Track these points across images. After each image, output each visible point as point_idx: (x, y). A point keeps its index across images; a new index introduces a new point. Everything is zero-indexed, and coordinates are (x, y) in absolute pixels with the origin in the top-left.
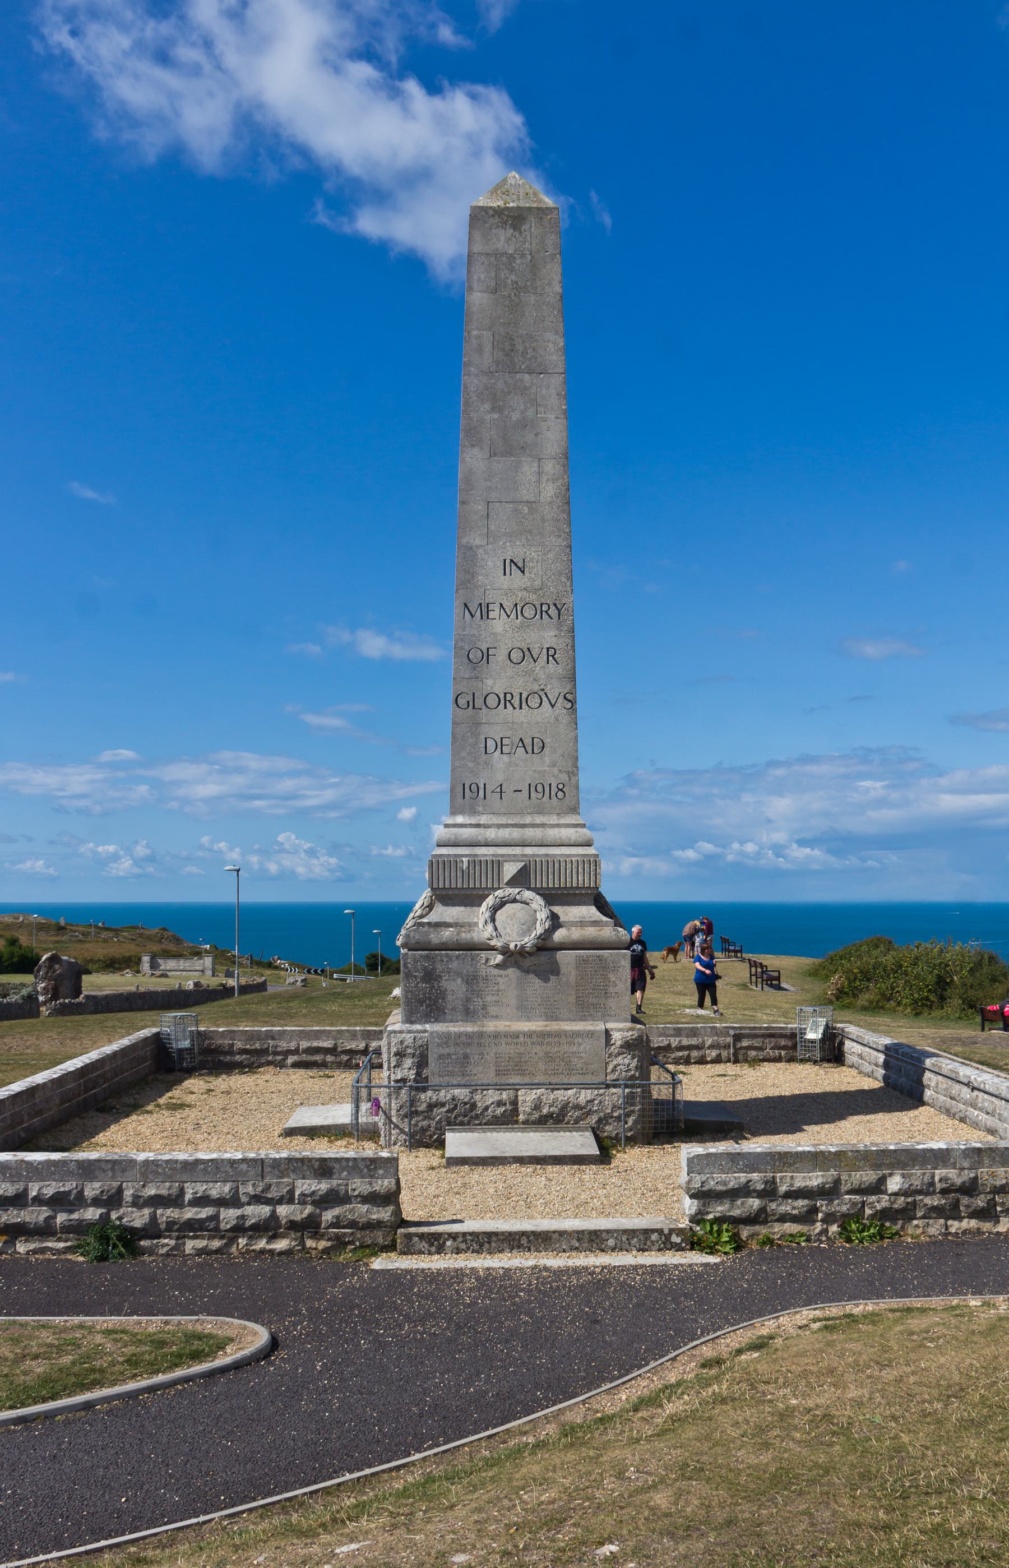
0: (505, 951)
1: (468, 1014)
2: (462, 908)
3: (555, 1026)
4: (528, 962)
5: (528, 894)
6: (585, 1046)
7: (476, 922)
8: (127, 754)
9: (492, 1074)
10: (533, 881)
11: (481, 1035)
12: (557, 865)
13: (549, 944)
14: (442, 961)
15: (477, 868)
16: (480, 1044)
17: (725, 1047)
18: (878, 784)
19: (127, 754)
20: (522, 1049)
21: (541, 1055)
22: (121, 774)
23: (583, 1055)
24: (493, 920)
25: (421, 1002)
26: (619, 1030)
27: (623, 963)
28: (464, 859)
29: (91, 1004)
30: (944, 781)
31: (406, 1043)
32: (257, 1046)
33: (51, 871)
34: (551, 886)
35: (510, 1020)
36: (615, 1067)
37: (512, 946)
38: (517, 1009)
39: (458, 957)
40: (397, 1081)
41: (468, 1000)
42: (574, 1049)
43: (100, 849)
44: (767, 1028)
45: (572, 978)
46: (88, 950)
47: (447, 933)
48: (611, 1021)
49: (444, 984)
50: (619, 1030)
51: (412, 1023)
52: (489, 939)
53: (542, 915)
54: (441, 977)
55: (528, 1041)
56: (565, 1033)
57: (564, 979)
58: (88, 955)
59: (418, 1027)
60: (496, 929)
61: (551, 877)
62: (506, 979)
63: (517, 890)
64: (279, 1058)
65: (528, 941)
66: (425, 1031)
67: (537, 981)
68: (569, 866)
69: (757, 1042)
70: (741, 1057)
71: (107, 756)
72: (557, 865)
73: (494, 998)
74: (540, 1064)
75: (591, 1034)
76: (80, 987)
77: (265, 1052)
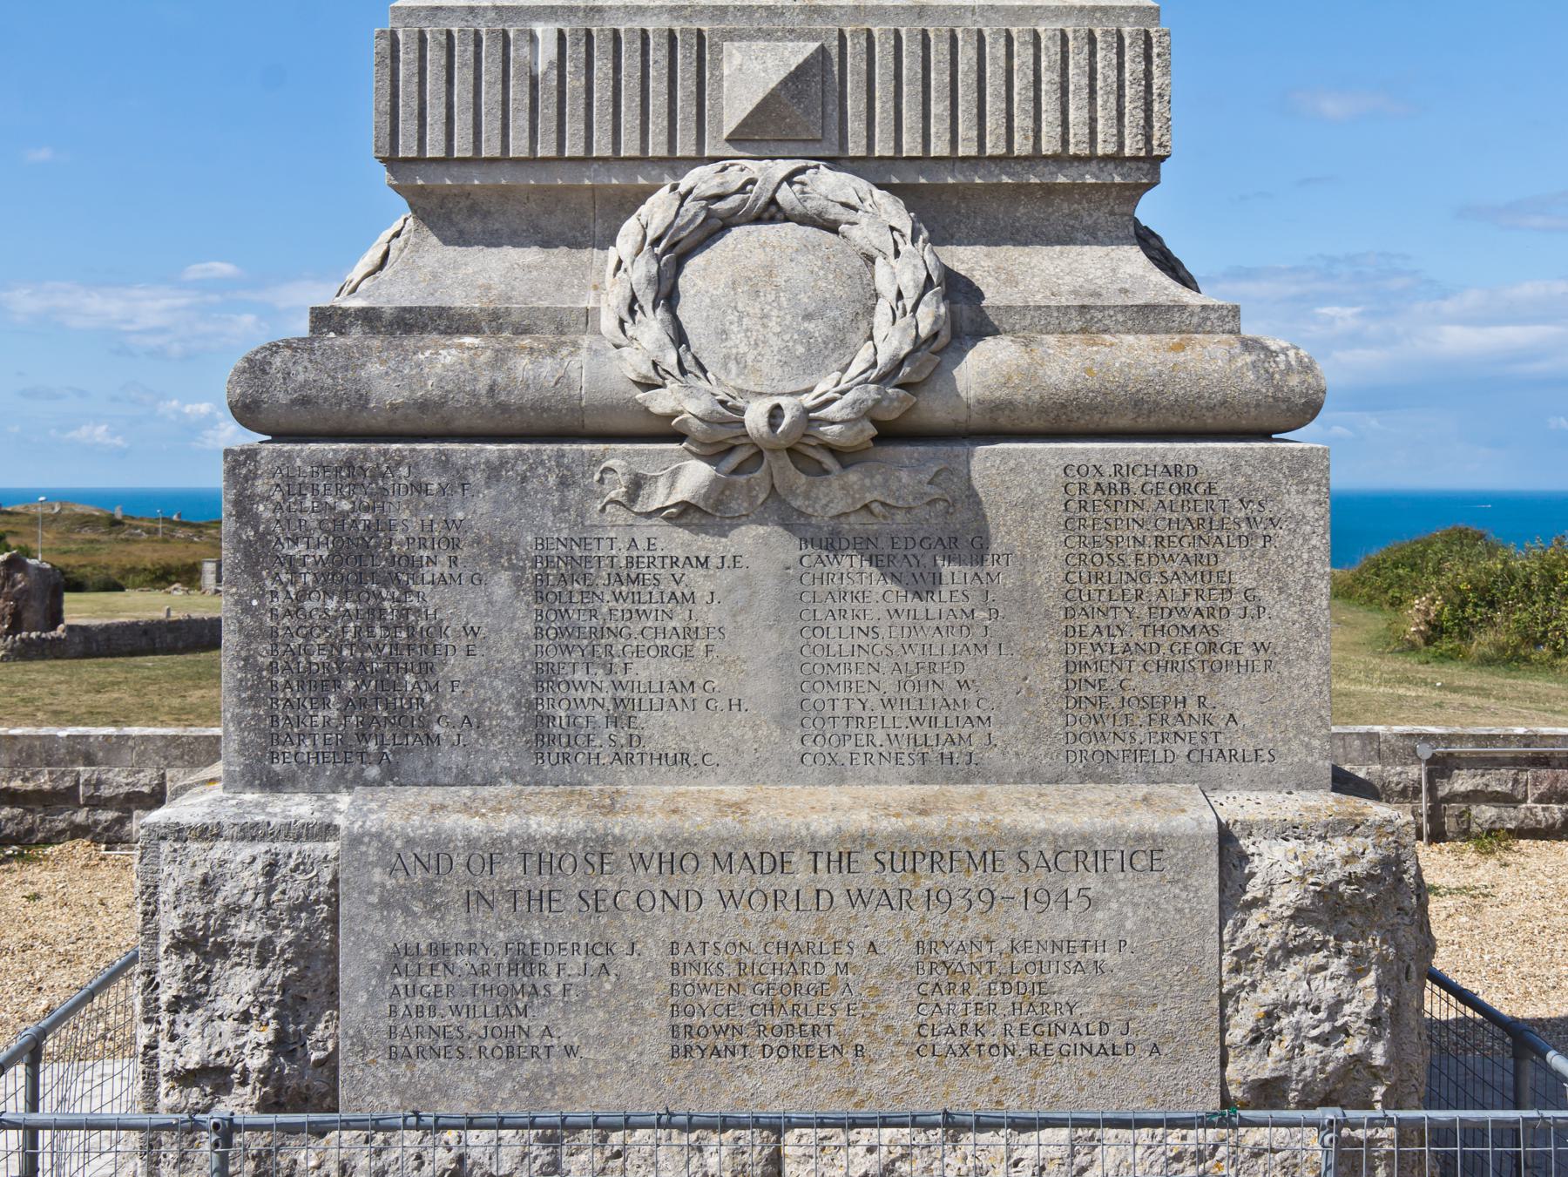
0: (723, 441)
1: (546, 746)
2: (532, 255)
3: (964, 810)
4: (835, 495)
5: (829, 186)
6: (1121, 908)
7: (594, 317)
8: (224, 268)
9: (654, 1042)
10: (855, 126)
11: (599, 852)
12: (966, 55)
13: (934, 410)
14: (420, 488)
15: (602, 67)
16: (593, 901)
17: (1403, 793)
18: (1349, 311)
19: (224, 268)
20: (803, 927)
21: (900, 954)
22: (215, 298)
23: (1109, 958)
24: (668, 297)
25: (319, 685)
26: (1287, 831)
27: (1293, 501)
28: (539, 29)
29: (77, 640)
30: (1448, 307)
31: (228, 891)
32: (44, 781)
33: (118, 441)
34: (939, 148)
35: (747, 776)
36: (1270, 1016)
37: (755, 417)
38: (782, 720)
39: (494, 472)
40: (185, 1078)
41: (545, 676)
42: (1064, 925)
43: (188, 409)
44: (1527, 740)
45: (1048, 575)
46: (129, 554)
47: (448, 357)
48: (1232, 782)
49: (429, 598)
50: (1287, 831)
51: (274, 784)
52: (647, 386)
53: (902, 272)
54: (412, 564)
55: (834, 882)
56: (1021, 846)
57: (1008, 579)
58: (127, 562)
59: (299, 807)
60: (679, 337)
61: (938, 108)
62: (727, 577)
63: (783, 167)
64: (106, 816)
65: (839, 391)
66: (327, 831)
67: (878, 586)
68: (1023, 56)
69: (1498, 781)
70: (1450, 824)
71: (195, 271)
72: (966, 55)
73: (670, 669)
74: (894, 1001)
75: (1148, 852)
76: (60, 611)
77: (65, 798)
